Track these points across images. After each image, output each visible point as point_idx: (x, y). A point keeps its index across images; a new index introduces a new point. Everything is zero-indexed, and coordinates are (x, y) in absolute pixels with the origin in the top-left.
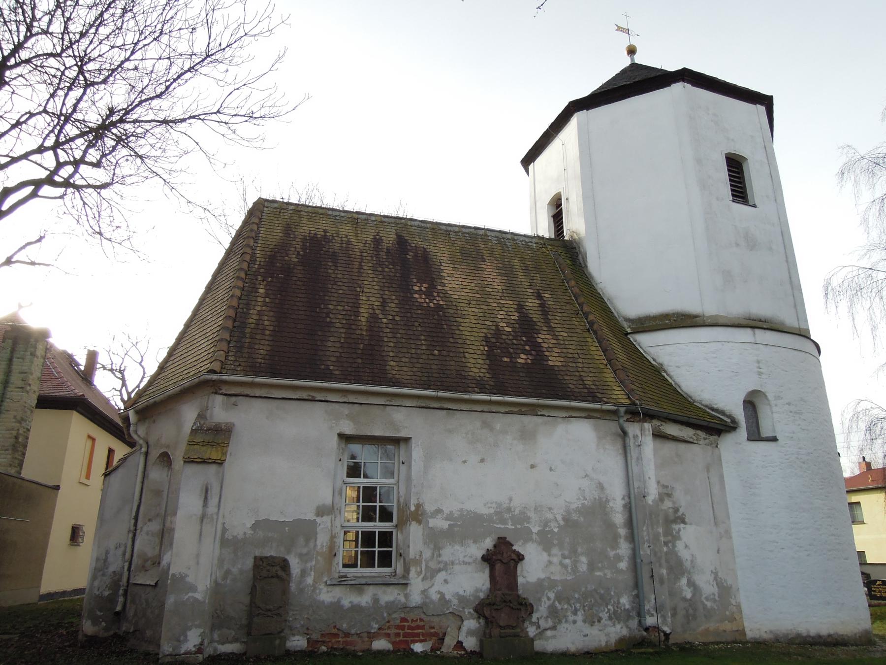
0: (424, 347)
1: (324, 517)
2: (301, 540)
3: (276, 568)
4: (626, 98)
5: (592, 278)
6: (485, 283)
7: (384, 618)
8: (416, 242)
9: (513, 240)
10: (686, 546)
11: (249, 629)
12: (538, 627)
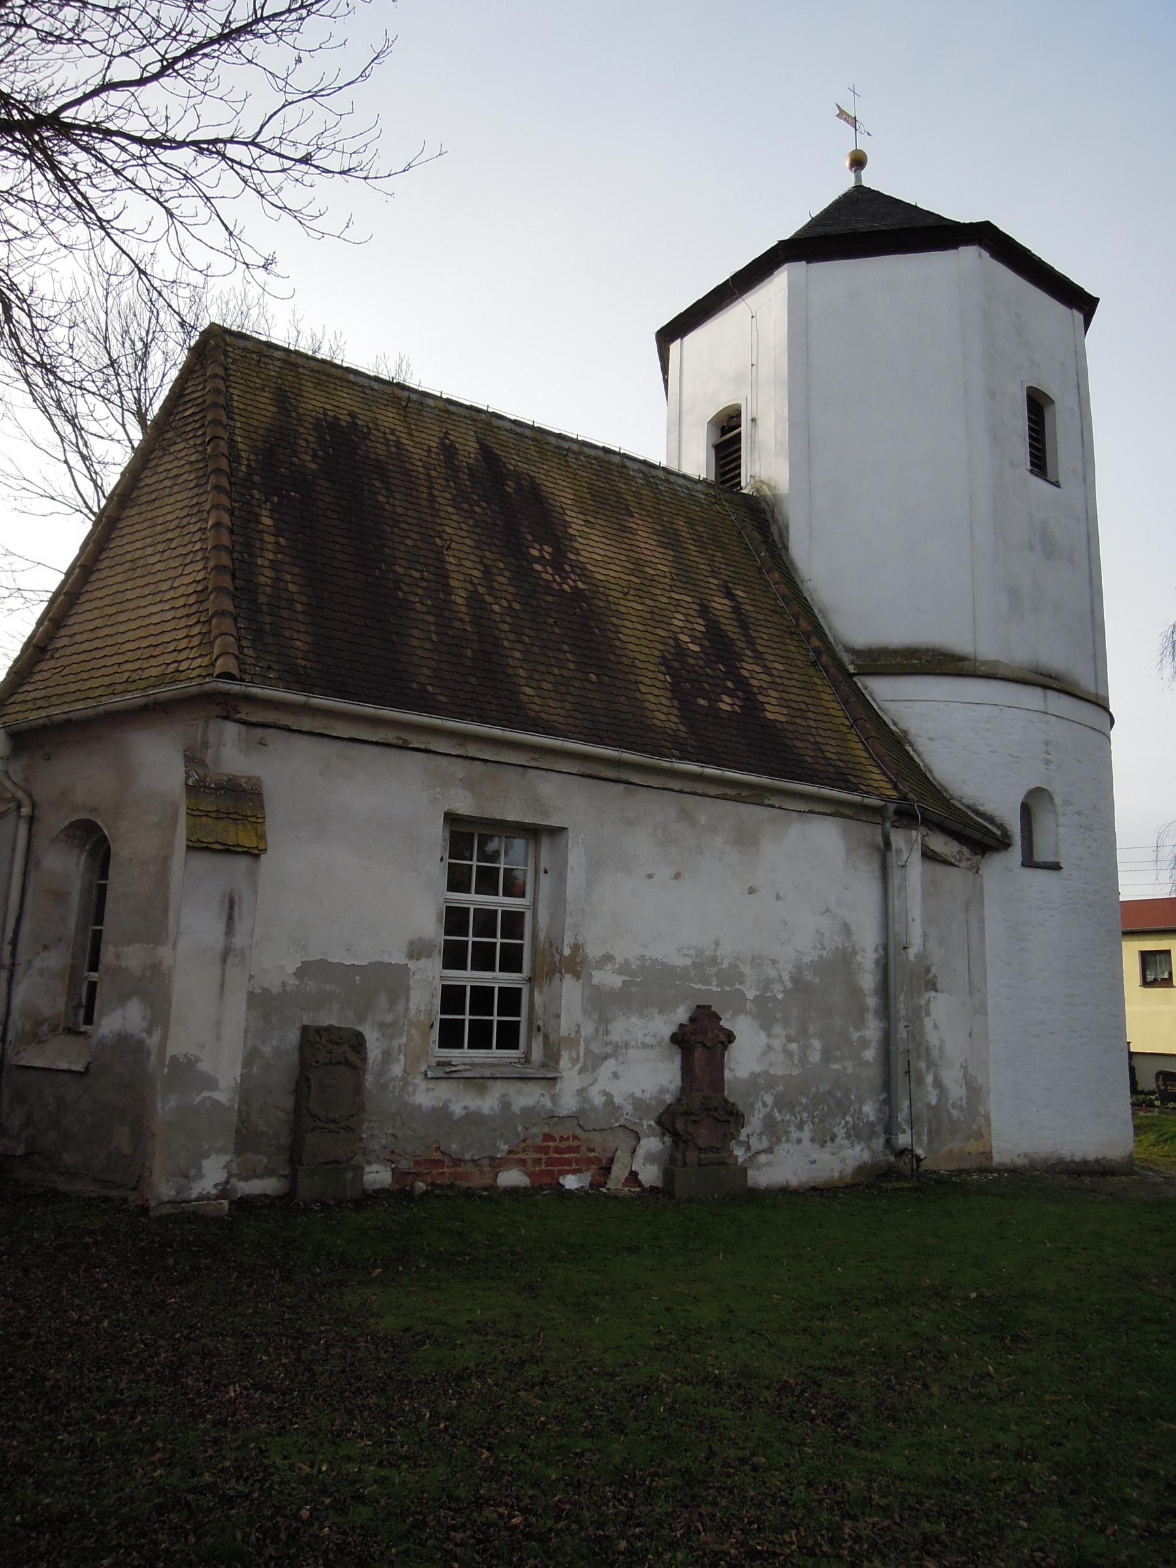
0: (571, 666)
1: (421, 961)
2: (383, 1001)
4: (878, 255)
5: (796, 569)
6: (642, 556)
7: (517, 1134)
8: (513, 461)
9: (667, 481)
10: (936, 1026)
11: (295, 1156)
12: (748, 1148)
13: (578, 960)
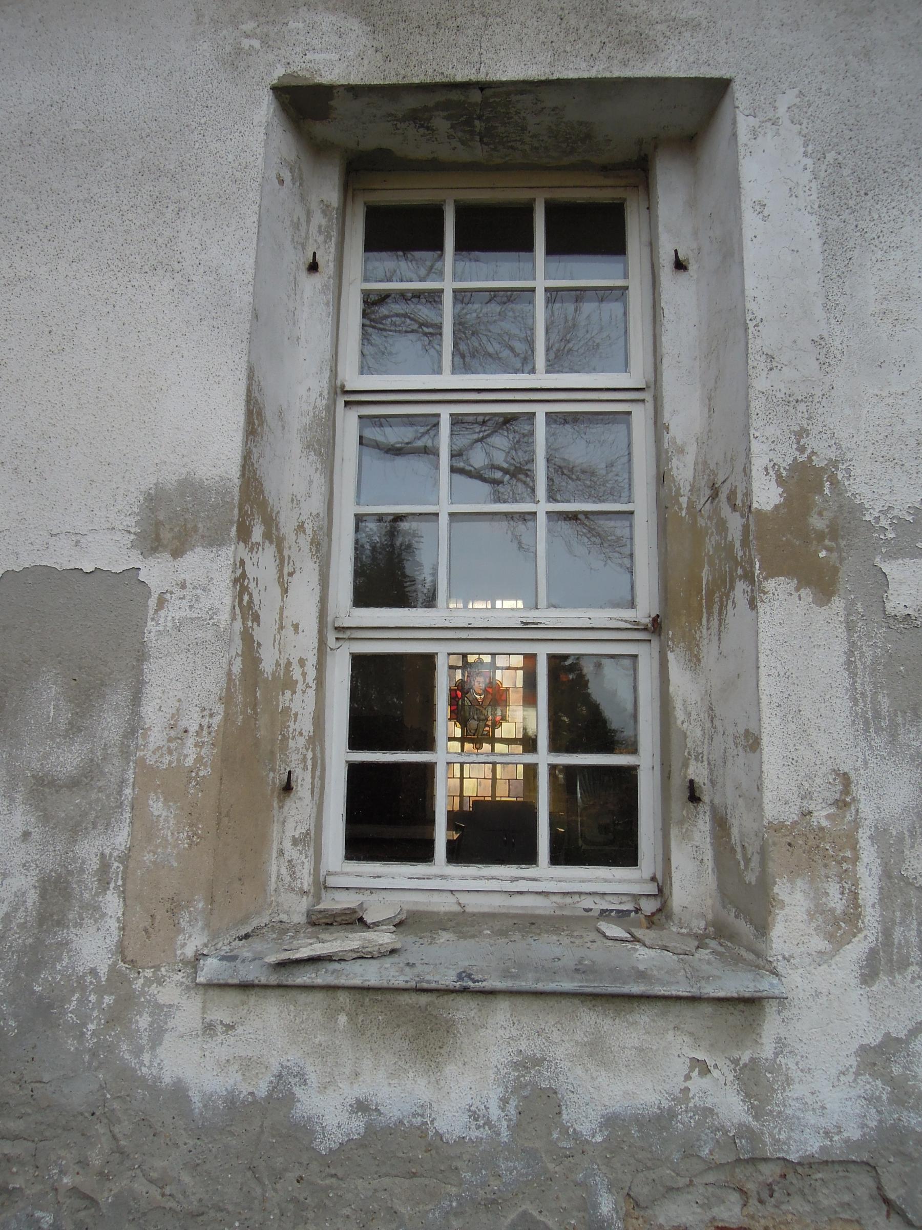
13: (818, 523)
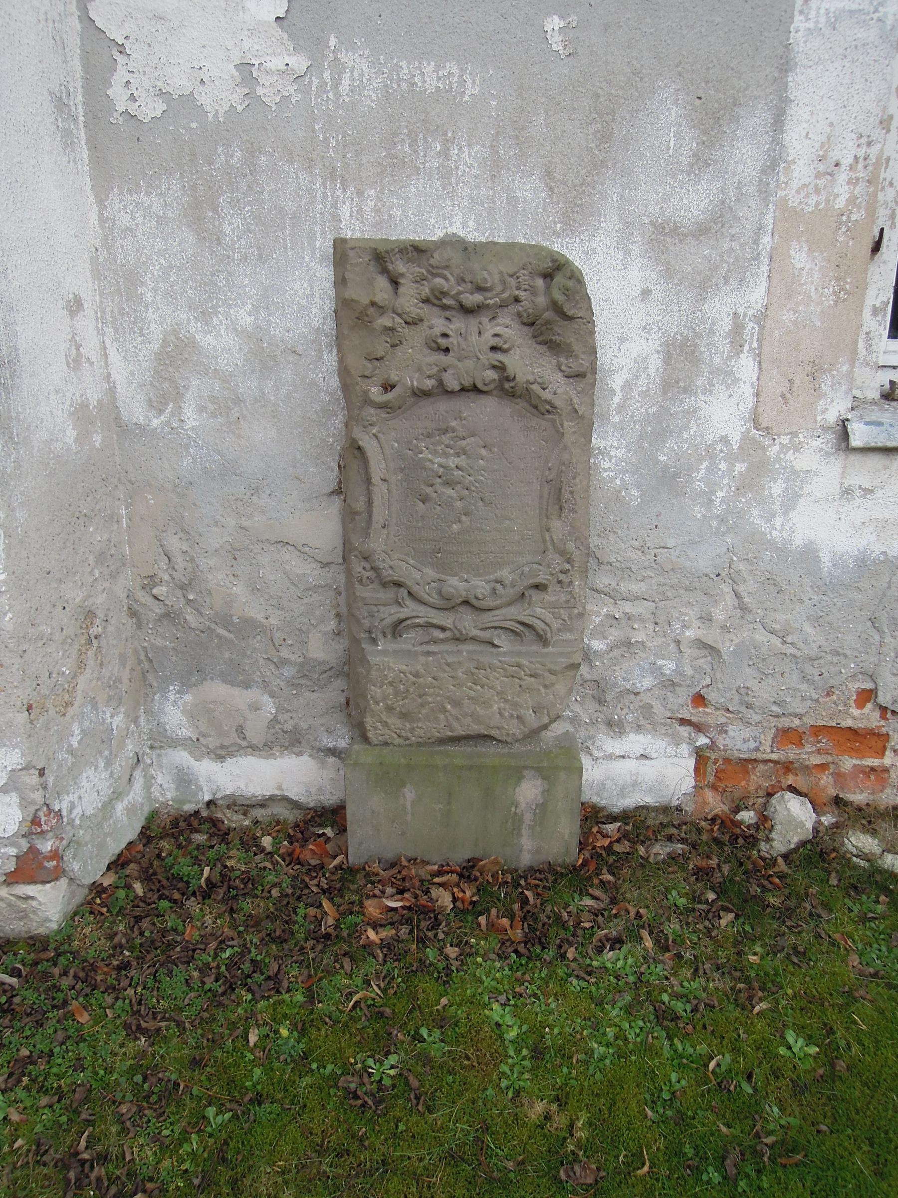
3: (490, 329)
7: (779, 435)
